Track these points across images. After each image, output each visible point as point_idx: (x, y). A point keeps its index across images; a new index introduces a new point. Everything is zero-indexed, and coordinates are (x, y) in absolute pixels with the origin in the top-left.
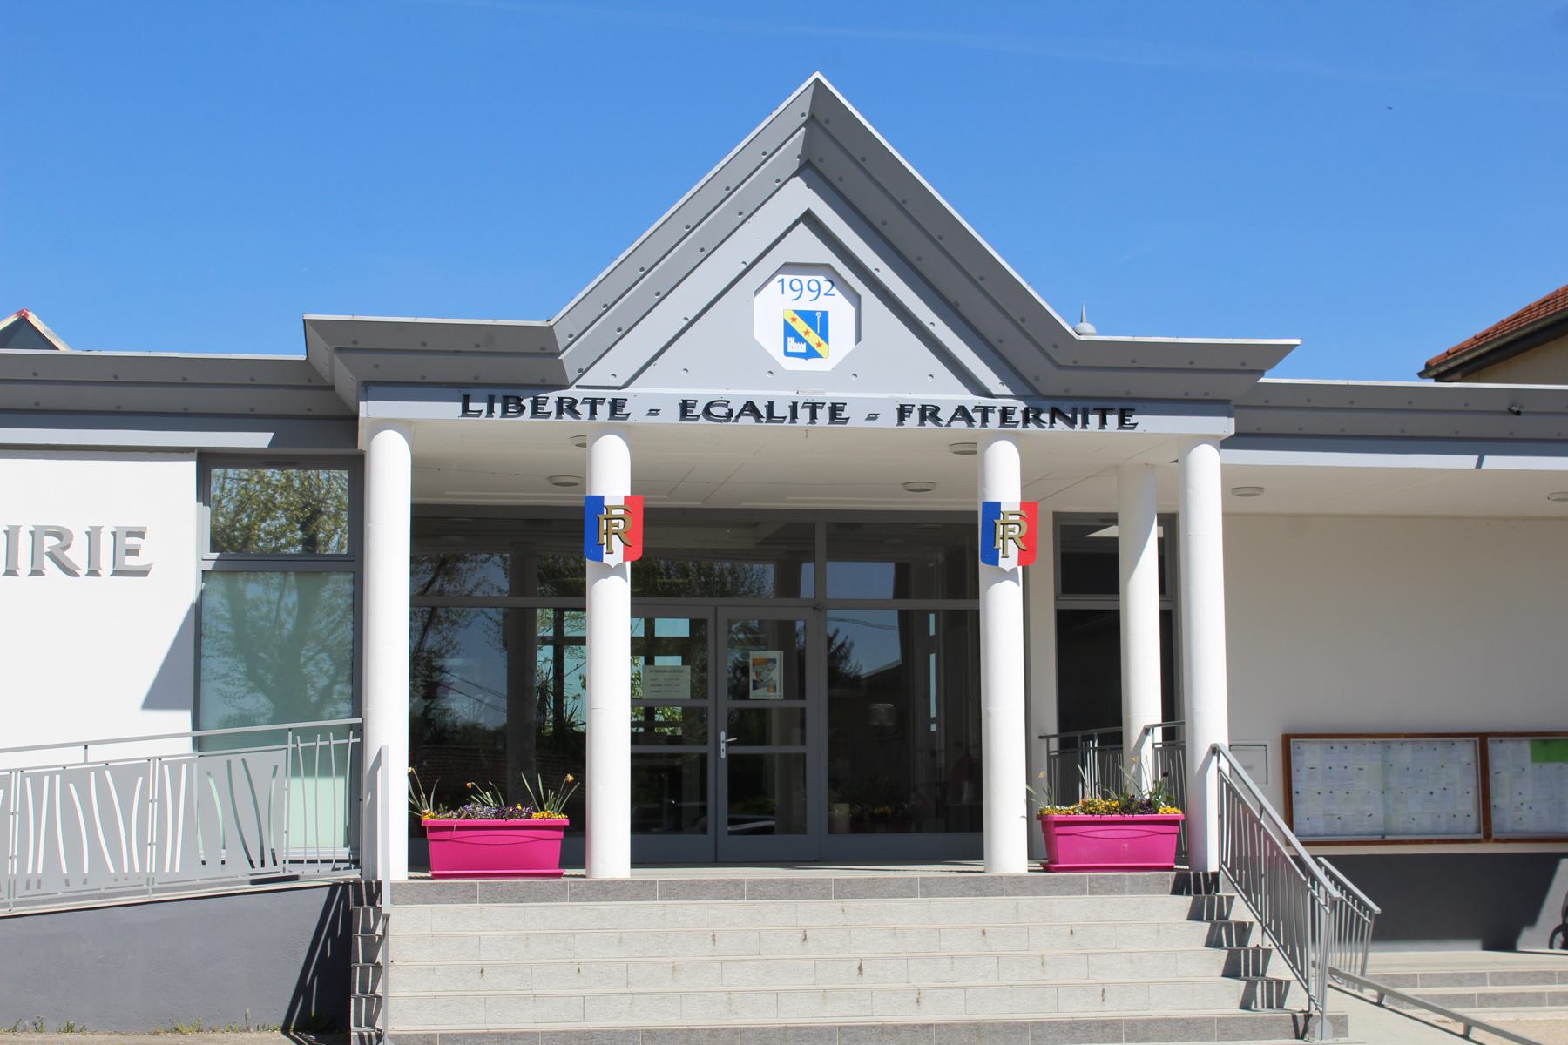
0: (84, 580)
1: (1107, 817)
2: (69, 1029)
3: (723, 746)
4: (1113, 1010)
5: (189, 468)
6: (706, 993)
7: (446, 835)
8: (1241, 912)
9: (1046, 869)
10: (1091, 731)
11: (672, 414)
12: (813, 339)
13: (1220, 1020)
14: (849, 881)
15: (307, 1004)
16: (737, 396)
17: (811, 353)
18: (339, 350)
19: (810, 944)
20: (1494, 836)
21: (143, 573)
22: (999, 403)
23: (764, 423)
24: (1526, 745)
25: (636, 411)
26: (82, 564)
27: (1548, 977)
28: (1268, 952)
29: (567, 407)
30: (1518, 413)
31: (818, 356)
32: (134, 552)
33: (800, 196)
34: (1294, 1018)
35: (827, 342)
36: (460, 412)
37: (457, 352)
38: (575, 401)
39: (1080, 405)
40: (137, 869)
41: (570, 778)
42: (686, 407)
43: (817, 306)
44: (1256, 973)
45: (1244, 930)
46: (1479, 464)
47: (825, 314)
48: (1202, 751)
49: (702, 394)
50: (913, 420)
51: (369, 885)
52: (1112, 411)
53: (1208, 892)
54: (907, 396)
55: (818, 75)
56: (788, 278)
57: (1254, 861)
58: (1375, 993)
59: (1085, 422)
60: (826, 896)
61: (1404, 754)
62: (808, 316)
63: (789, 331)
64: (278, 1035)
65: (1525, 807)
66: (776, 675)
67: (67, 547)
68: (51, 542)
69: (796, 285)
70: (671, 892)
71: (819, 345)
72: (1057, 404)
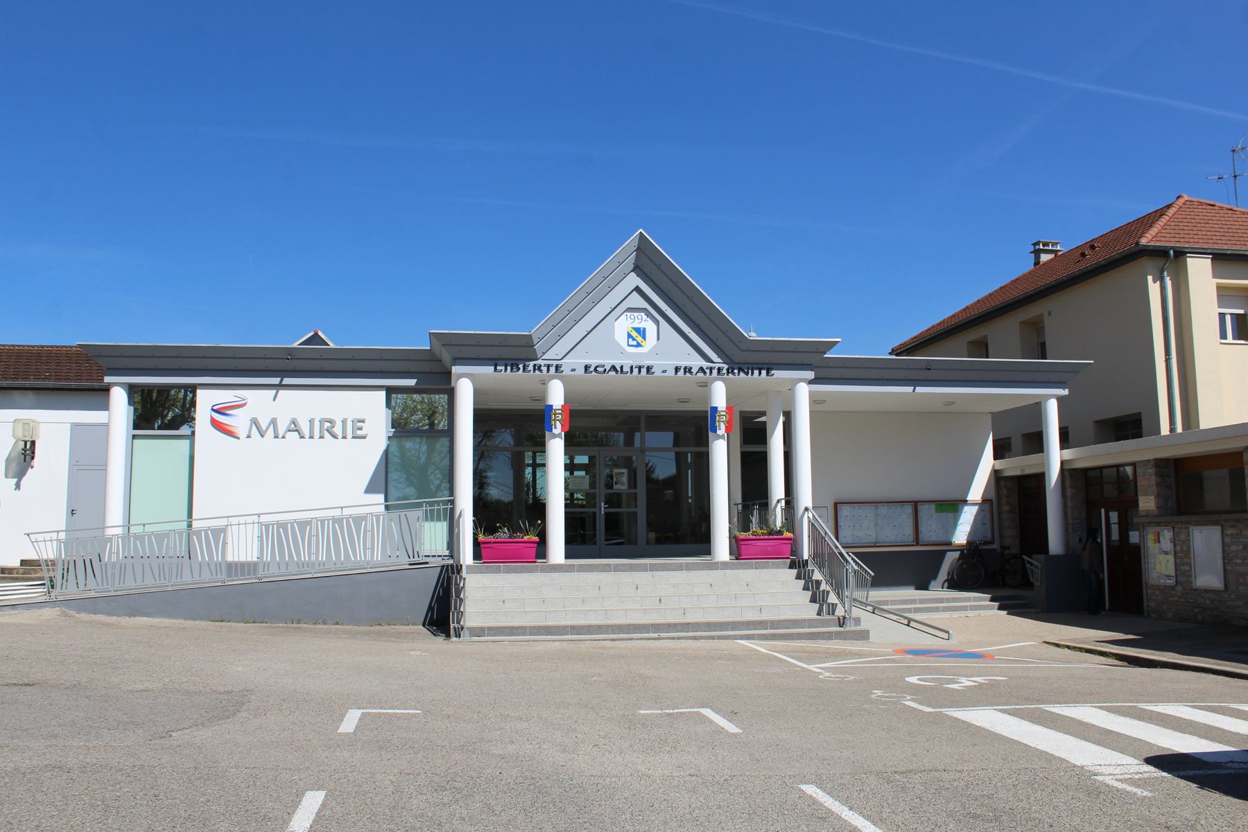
0: (340, 440)
1: (762, 537)
2: (337, 624)
3: (603, 509)
4: (765, 616)
6: (595, 611)
9: (737, 559)
12: (640, 339)
14: (656, 564)
15: (432, 615)
17: (639, 345)
18: (444, 345)
19: (639, 590)
20: (920, 543)
21: (364, 437)
22: (717, 366)
24: (933, 506)
25: (566, 370)
26: (306, 432)
27: (941, 600)
28: (828, 592)
30: (929, 369)
31: (641, 346)
32: (361, 429)
33: (634, 280)
34: (839, 618)
35: (645, 340)
37: (492, 346)
38: (541, 366)
41: (539, 522)
42: (587, 368)
43: (641, 326)
45: (818, 583)
47: (644, 329)
49: (594, 362)
50: (681, 373)
51: (457, 566)
54: (678, 363)
55: (641, 230)
56: (629, 314)
58: (872, 608)
59: (753, 373)
61: (884, 510)
62: (637, 330)
63: (629, 336)
64: (421, 627)
66: (625, 479)
67: (334, 427)
68: (327, 425)
69: (632, 317)
70: (582, 569)
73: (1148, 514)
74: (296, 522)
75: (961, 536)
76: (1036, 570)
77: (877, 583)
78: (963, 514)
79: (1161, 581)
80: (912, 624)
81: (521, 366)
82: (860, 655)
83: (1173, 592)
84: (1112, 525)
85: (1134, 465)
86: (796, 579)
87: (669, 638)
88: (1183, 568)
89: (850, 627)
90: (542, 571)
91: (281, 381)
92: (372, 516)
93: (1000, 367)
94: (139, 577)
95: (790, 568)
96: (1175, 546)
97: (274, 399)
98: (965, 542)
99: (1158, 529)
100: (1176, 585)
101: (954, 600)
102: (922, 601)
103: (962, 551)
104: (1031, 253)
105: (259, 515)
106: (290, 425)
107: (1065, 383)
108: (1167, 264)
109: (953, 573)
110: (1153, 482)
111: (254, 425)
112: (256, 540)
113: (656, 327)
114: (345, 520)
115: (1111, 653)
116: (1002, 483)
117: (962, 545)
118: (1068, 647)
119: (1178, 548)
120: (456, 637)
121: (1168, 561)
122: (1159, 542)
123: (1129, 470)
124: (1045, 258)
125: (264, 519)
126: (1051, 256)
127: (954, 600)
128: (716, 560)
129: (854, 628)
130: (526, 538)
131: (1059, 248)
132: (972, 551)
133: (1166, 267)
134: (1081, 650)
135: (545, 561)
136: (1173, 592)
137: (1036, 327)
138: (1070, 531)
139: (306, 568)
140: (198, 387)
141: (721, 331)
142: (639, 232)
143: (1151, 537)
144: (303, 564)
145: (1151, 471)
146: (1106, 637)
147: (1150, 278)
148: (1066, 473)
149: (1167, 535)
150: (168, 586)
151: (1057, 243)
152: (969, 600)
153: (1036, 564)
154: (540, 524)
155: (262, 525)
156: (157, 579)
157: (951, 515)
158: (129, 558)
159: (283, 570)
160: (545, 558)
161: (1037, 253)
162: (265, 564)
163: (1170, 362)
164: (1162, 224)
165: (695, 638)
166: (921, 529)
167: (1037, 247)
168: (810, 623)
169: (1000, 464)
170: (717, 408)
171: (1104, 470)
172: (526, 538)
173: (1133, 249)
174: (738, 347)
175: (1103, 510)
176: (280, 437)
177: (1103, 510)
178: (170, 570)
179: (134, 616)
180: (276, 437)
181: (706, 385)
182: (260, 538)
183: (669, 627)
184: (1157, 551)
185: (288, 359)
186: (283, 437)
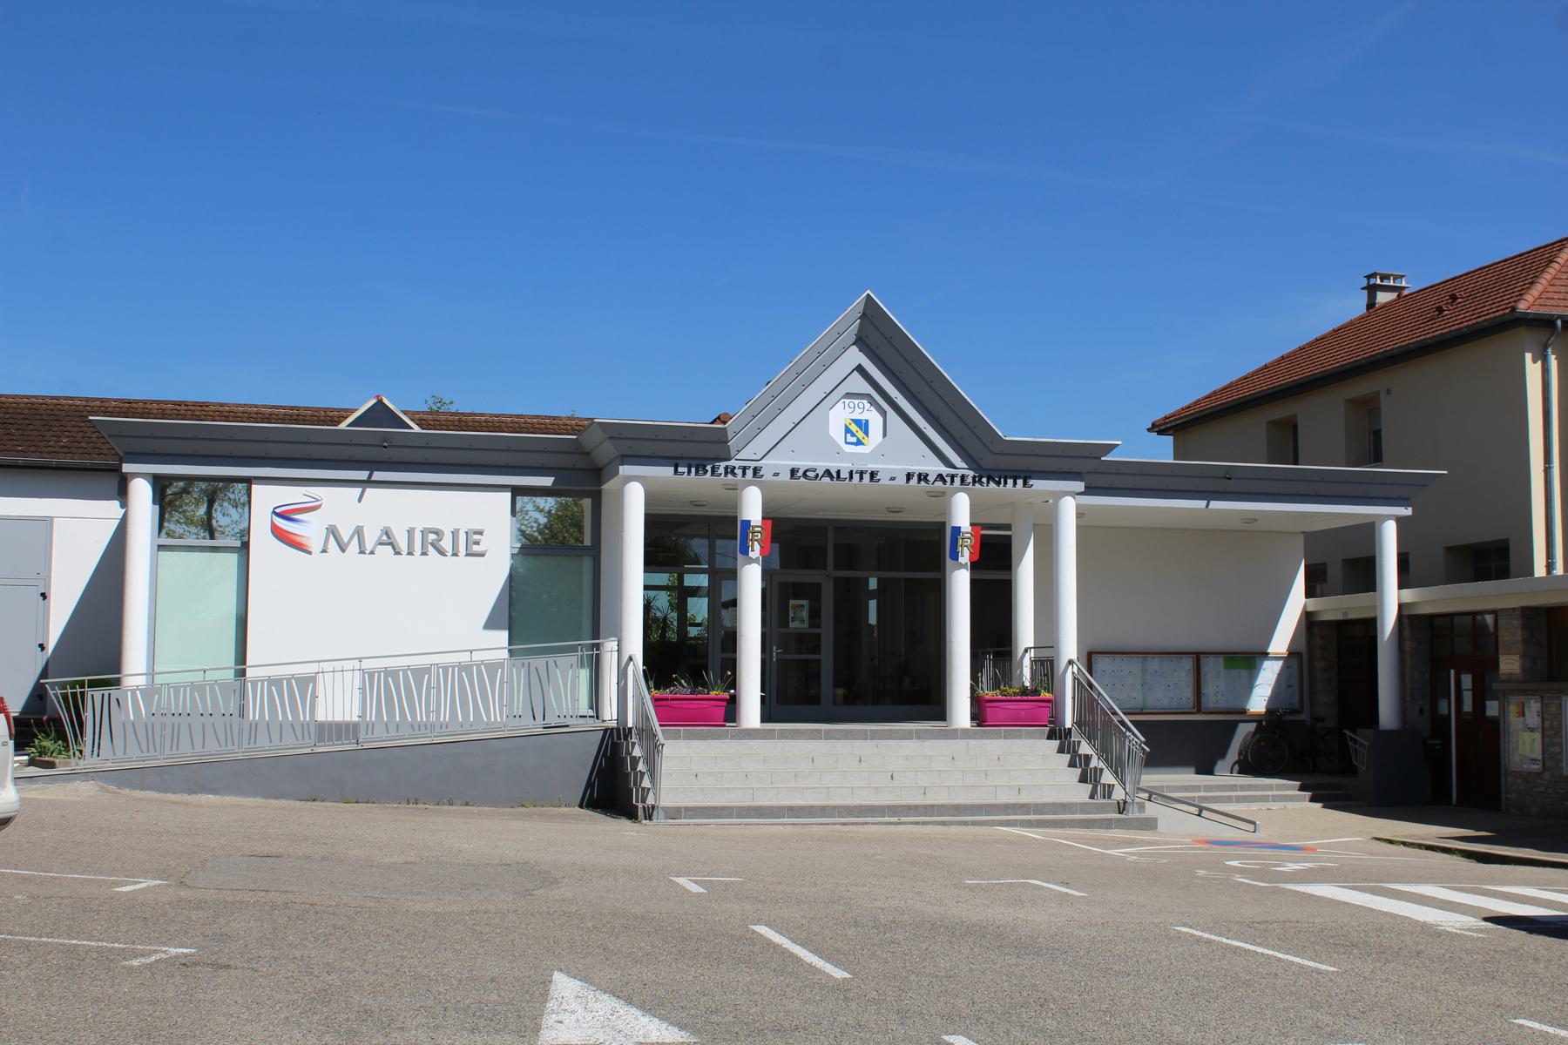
0: (450, 559)
1: (1014, 698)
2: (467, 804)
3: (774, 654)
4: (1025, 798)
5: (508, 495)
6: (815, 788)
7: (665, 703)
8: (1085, 748)
9: (979, 725)
10: (988, 649)
11: (785, 476)
12: (860, 434)
13: (1081, 804)
14: (878, 731)
15: (592, 793)
16: (821, 466)
17: (859, 443)
18: (610, 438)
19: (863, 764)
20: (1203, 710)
21: (482, 555)
22: (960, 472)
23: (835, 481)
24: (1221, 660)
25: (767, 474)
26: (404, 548)
27: (1233, 788)
28: (1102, 770)
29: (730, 471)
30: (1230, 479)
31: (863, 444)
32: (477, 543)
33: (856, 356)
34: (1118, 803)
35: (867, 436)
36: (673, 473)
37: (673, 440)
38: (735, 468)
39: (1003, 474)
40: (499, 720)
41: (729, 673)
42: (793, 472)
43: (862, 417)
44: (1095, 780)
45: (1088, 758)
46: (1207, 506)
47: (867, 421)
48: (1064, 663)
49: (802, 464)
50: (914, 481)
51: (624, 729)
52: (1020, 478)
53: (1066, 738)
54: (912, 468)
55: (869, 292)
56: (847, 401)
57: (1094, 723)
58: (1147, 795)
59: (1006, 483)
60: (866, 739)
61: (1154, 664)
62: (857, 422)
63: (848, 430)
64: (577, 808)
65: (1220, 694)
66: (805, 614)
67: (441, 540)
68: (432, 537)
69: (852, 405)
70: (783, 735)
71: (857, 431)
72: (990, 473)
73: (1510, 679)
74: (294, 679)
75: (1258, 702)
76: (1362, 749)
77: (1155, 760)
78: (1262, 671)
79: (1525, 766)
80: (1205, 813)
81: (709, 468)
82: (1150, 843)
83: (1539, 781)
84: (1464, 692)
85: (1495, 612)
86: (1058, 752)
87: (912, 823)
88: (1552, 749)
89: (1132, 814)
90: (733, 737)
91: (370, 476)
92: (438, 668)
93: (1324, 477)
94: (275, 737)
95: (1048, 738)
96: (1543, 721)
97: (360, 500)
98: (1264, 710)
99: (1523, 698)
100: (1543, 771)
101: (1250, 787)
102: (1209, 788)
103: (1259, 722)
104: (1362, 289)
105: (360, 660)
106: (381, 536)
107: (1407, 499)
108: (1552, 339)
109: (1246, 752)
110: (1519, 638)
111: (332, 537)
112: (357, 693)
113: (882, 419)
114: (475, 667)
115: (1457, 850)
116: (1316, 630)
117: (1259, 715)
118: (1404, 844)
119: (1547, 724)
120: (646, 819)
121: (1534, 740)
122: (1523, 715)
123: (1489, 619)
124: (1383, 298)
125: (366, 664)
126: (1390, 296)
127: (1250, 787)
128: (955, 727)
129: (1137, 815)
130: (713, 694)
131: (1404, 284)
132: (1272, 722)
133: (1550, 342)
134: (1420, 846)
135: (735, 724)
136: (1539, 781)
137: (1368, 408)
138: (1408, 698)
139: (423, 731)
140: (253, 481)
141: (969, 427)
142: (866, 294)
143: (1513, 709)
144: (419, 726)
145: (1517, 622)
146: (1450, 833)
147: (1528, 356)
148: (1405, 621)
149: (1534, 706)
150: (238, 753)
151: (1402, 277)
152: (1270, 788)
153: (1361, 740)
154: (730, 675)
155: (364, 673)
156: (223, 743)
157: (1244, 673)
158: (184, 715)
159: (393, 733)
160: (735, 721)
161: (1372, 290)
162: (368, 725)
163: (1550, 473)
164: (1548, 277)
165: (944, 824)
166: (1204, 691)
167: (1372, 281)
168: (1083, 808)
169: (1314, 604)
170: (959, 528)
171: (1456, 618)
172: (713, 694)
173: (1507, 317)
174: (989, 449)
175: (1452, 672)
176: (367, 552)
177: (1452, 672)
178: (241, 732)
179: (196, 793)
180: (362, 552)
181: (943, 499)
182: (363, 689)
183: (909, 809)
184: (1521, 727)
185: (385, 447)
186: (372, 553)
